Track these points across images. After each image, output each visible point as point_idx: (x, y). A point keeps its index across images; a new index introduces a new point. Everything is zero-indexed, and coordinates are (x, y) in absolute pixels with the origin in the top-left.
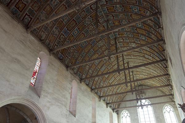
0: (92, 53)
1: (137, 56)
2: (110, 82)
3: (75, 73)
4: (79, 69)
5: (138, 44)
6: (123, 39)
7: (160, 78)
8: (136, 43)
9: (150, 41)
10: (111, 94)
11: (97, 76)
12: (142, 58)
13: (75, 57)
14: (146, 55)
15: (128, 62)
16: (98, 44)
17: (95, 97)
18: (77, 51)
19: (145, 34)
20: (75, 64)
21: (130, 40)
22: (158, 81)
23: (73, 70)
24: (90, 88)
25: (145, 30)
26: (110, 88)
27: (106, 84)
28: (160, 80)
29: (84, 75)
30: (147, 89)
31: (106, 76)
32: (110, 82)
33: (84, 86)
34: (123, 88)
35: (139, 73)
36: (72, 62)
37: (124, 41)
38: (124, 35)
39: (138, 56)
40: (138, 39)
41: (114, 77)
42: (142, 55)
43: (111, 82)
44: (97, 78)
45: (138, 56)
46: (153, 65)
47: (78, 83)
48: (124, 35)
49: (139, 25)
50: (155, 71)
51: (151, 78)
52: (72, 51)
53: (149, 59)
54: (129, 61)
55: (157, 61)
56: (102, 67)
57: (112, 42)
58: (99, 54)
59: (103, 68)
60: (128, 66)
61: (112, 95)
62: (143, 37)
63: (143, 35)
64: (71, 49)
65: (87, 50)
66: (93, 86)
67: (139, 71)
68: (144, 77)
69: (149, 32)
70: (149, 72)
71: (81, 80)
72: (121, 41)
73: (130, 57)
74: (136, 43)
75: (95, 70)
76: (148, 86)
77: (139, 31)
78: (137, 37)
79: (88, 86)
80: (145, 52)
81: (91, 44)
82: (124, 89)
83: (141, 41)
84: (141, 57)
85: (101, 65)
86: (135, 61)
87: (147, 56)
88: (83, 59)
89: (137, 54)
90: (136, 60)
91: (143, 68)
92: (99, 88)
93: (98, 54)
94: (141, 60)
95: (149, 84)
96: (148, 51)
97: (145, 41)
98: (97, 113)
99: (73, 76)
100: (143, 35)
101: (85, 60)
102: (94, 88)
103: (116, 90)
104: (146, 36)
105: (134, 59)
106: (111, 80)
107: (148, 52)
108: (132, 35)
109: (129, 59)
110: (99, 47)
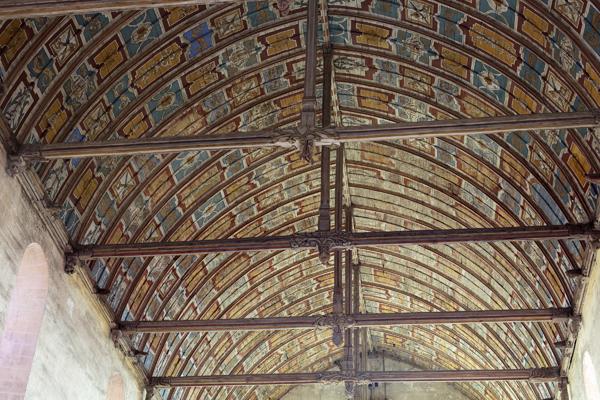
0: (174, 98)
1: (416, 178)
2: (225, 301)
3: (52, 196)
4: (75, 177)
6: (369, 62)
7: (499, 326)
8: (436, 104)
9: (526, 103)
10: (209, 372)
11: (164, 245)
12: (442, 196)
13: (68, 98)
14: (471, 188)
15: (353, 205)
16: (220, 53)
17: (125, 373)
18: (91, 61)
19: (513, 60)
20: (61, 142)
21: (407, 82)
22: (480, 345)
23: (40, 174)
24: (110, 310)
25: (520, 41)
26: (214, 336)
27: (199, 307)
28: (493, 341)
29: (92, 227)
30: (401, 375)
31: (212, 261)
32: (225, 301)
33: (79, 298)
34: (279, 351)
35: (392, 284)
36: (49, 126)
37: (369, 75)
38: (384, 45)
39: (421, 181)
40: (455, 80)
41: (251, 280)
42: (441, 183)
43: (227, 304)
44: (158, 262)
45: (421, 181)
46: (485, 244)
47: (53, 265)
48: (384, 45)
49: (484, 82)
50: (488, 285)
51: (442, 316)
52: (62, 52)
53: (476, 211)
54: (359, 201)
55: (523, 228)
56: (201, 201)
58: (210, 118)
59: (207, 213)
61: (213, 377)
62: (488, 80)
63: (493, 62)
64: (63, 38)
66: (128, 306)
67: (397, 268)
68: (407, 305)
69: (536, 58)
70: (446, 286)
71: (73, 254)
72: (357, 72)
73: (371, 182)
74: (436, 104)
75: (163, 212)
76: (413, 363)
77: (478, 40)
79: (103, 301)
80: (469, 166)
81: (184, 46)
82: (283, 359)
83: (472, 98)
84: (433, 191)
85: (201, 185)
87: (468, 192)
88: (111, 126)
89: (415, 172)
90: (398, 200)
91: (416, 251)
92: (157, 324)
93: (205, 114)
94: (429, 211)
95: (422, 351)
96: (492, 167)
99: (32, 217)
100: (493, 62)
101: (121, 132)
102: (132, 318)
103: (240, 358)
104: (551, 62)
105: (392, 198)
106: (232, 289)
107: (486, 171)
108: (430, 52)
109: (365, 192)
110: (221, 77)
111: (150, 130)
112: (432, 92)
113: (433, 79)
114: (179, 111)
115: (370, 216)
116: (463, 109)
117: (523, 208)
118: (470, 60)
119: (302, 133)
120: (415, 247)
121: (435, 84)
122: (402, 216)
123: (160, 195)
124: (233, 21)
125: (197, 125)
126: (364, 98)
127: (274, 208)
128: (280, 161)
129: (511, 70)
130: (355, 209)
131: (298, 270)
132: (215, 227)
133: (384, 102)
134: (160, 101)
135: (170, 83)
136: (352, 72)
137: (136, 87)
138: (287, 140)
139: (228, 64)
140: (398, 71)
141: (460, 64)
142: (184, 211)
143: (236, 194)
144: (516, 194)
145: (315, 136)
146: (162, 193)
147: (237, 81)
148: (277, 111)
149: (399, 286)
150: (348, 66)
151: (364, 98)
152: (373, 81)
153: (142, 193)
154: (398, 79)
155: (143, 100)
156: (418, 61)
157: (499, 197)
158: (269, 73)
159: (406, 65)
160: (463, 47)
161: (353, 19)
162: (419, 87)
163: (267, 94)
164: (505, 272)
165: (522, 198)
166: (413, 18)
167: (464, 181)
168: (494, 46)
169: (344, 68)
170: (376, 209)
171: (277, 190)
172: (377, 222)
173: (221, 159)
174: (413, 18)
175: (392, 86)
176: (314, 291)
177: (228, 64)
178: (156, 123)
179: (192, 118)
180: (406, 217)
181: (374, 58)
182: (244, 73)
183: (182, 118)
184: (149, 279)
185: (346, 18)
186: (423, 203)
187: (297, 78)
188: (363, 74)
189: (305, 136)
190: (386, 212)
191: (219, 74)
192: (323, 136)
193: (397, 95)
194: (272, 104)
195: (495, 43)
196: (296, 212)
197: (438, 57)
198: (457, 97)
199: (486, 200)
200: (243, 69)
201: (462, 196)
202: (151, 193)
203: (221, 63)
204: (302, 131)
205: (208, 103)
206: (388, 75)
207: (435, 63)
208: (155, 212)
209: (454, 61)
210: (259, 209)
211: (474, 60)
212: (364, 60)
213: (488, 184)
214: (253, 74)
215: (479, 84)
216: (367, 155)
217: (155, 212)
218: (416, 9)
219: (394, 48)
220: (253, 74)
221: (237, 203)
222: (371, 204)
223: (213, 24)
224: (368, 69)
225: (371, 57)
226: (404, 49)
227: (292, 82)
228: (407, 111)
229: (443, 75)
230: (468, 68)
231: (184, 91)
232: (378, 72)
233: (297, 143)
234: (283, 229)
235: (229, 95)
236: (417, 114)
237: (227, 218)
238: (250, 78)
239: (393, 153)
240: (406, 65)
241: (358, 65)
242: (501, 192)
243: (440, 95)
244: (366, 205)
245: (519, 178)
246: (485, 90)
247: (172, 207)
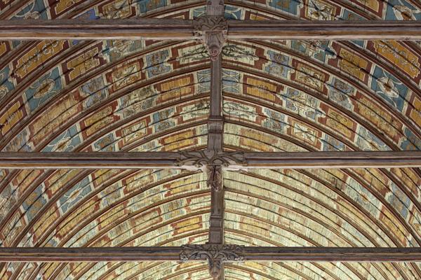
5: (342, 110)
6: (260, 53)
12: (323, 188)
14: (357, 185)
15: (226, 188)
21: (299, 76)
37: (257, 65)
49: (383, 88)
53: (359, 208)
57: (186, 51)
60: (217, 226)
62: (388, 86)
63: (394, 71)
65: (32, 66)
72: (246, 60)
74: (328, 101)
78: (353, 71)
83: (366, 100)
84: (314, 183)
86: (266, 194)
90: (275, 187)
93: (82, 99)
94: (307, 201)
97: (390, 108)
98: (117, 59)
100: (394, 71)
105: (268, 185)
108: (328, 51)
111: (25, 119)
112: (325, 88)
113: (327, 77)
114: (56, 97)
115: (242, 200)
116: (357, 110)
117: (411, 213)
118: (370, 65)
119: (210, 158)
120: (306, 263)
121: (330, 82)
122: (278, 203)
123: (27, 183)
124: (121, 8)
125: (73, 111)
126: (251, 86)
127: (142, 190)
128: (153, 144)
129: (413, 82)
130: (227, 192)
131: (138, 228)
132: (78, 212)
133: (272, 92)
134: (38, 90)
135: (51, 71)
136: (240, 60)
137: (16, 77)
138: (194, 164)
139: (111, 49)
140: (290, 64)
141: (359, 67)
142: (49, 198)
143: (104, 177)
144: (405, 199)
145: (224, 162)
146: (30, 181)
147: (118, 66)
148: (156, 95)
149: (265, 270)
150: (236, 54)
151: (251, 86)
152: (262, 71)
153: (11, 184)
154: (290, 72)
155: (21, 89)
156: (313, 57)
157: (386, 198)
158: (153, 57)
159: (300, 60)
160: (364, 51)
161: (248, 10)
162: (311, 83)
163: (148, 78)
164: (385, 270)
165: (412, 204)
166: (313, 16)
167: (349, 178)
168: (396, 56)
169: (232, 56)
170: (248, 194)
171: (147, 173)
172: (249, 207)
173: (92, 144)
174: (313, 16)
175: (282, 78)
176: (173, 272)
177: (111, 49)
178: (31, 111)
179: (68, 104)
180: (281, 204)
181: (266, 49)
182: (127, 58)
183: (57, 104)
184: (9, 269)
185: (239, 9)
186: (302, 193)
187: (181, 63)
188: (252, 63)
189: (212, 161)
190: (259, 197)
191: (101, 59)
192: (231, 162)
193: (286, 87)
194: (153, 88)
195: (398, 53)
196: (164, 194)
197: (335, 57)
198: (352, 97)
199: (371, 198)
200: (126, 54)
201: (346, 191)
202: (19, 182)
203: (104, 48)
204: (210, 155)
205: (86, 88)
206: (279, 67)
207: (331, 62)
208: (22, 201)
209: (352, 63)
210: (126, 192)
211: (404, 113)
212: (254, 50)
213: (376, 184)
214: (136, 59)
215: (377, 88)
216: (246, 141)
217: (22, 201)
218: (316, 9)
219: (288, 42)
220: (136, 59)
221: (104, 187)
222: (245, 188)
223: (100, 11)
224: (258, 59)
225: (263, 47)
226: (300, 44)
227: (175, 68)
228: (296, 104)
229: (339, 74)
230: (367, 72)
231: (63, 77)
232: (269, 63)
233: (204, 168)
234: (148, 211)
235: (108, 81)
236: (306, 108)
237: (92, 202)
238: (133, 62)
239: (275, 141)
240: (300, 60)
241: (247, 54)
242: (388, 195)
243: (334, 92)
244: (239, 189)
245: (410, 184)
246: (383, 95)
247: (38, 195)
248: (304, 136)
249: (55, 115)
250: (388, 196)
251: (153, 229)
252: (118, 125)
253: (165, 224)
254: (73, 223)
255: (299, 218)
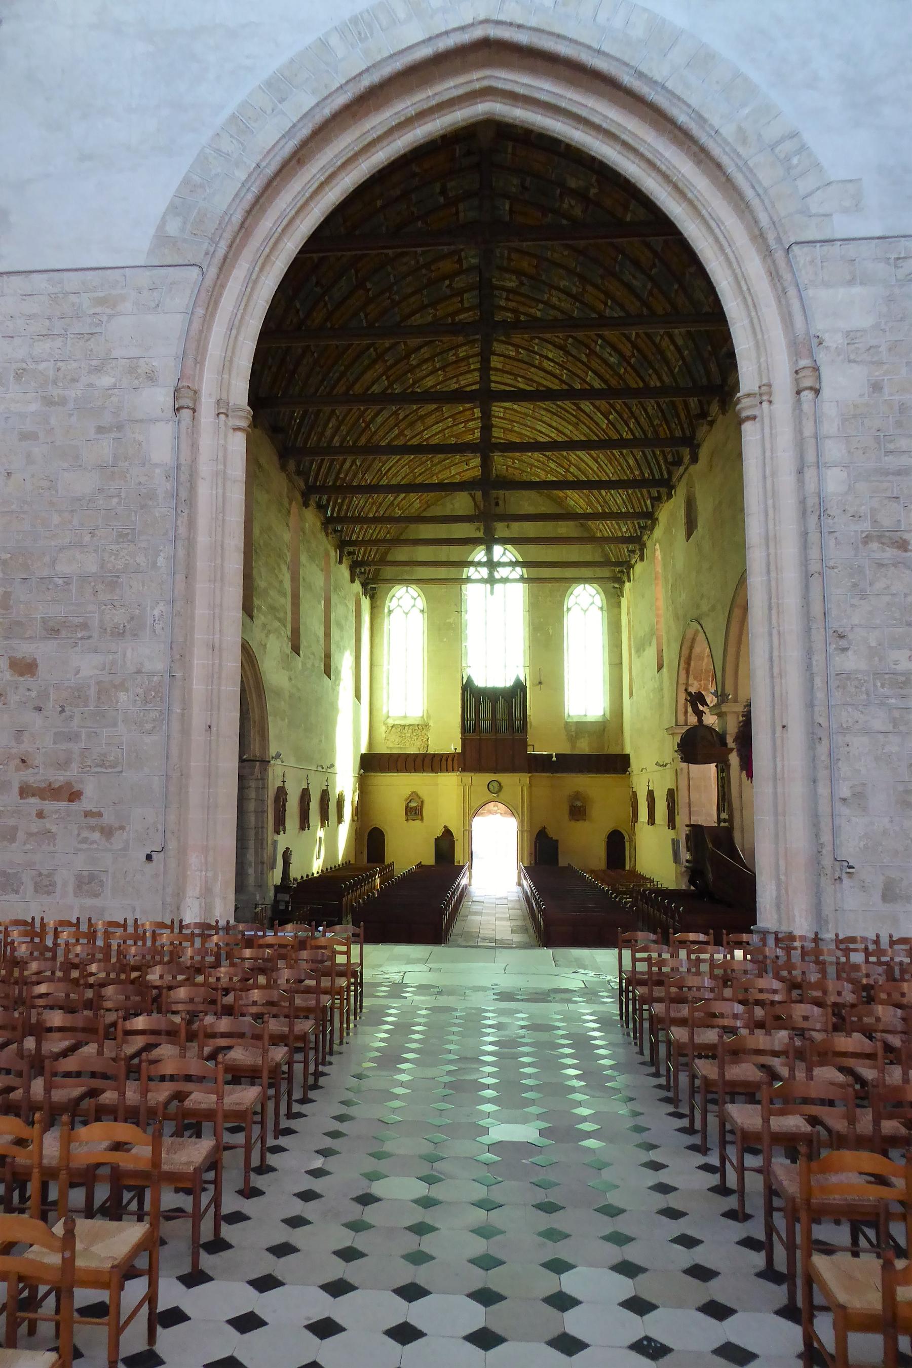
60: (487, 428)
248: (551, 368)
249: (369, 376)
250: (611, 417)
251: (437, 423)
252: (412, 369)
253: (447, 418)
254: (381, 433)
255: (549, 415)
